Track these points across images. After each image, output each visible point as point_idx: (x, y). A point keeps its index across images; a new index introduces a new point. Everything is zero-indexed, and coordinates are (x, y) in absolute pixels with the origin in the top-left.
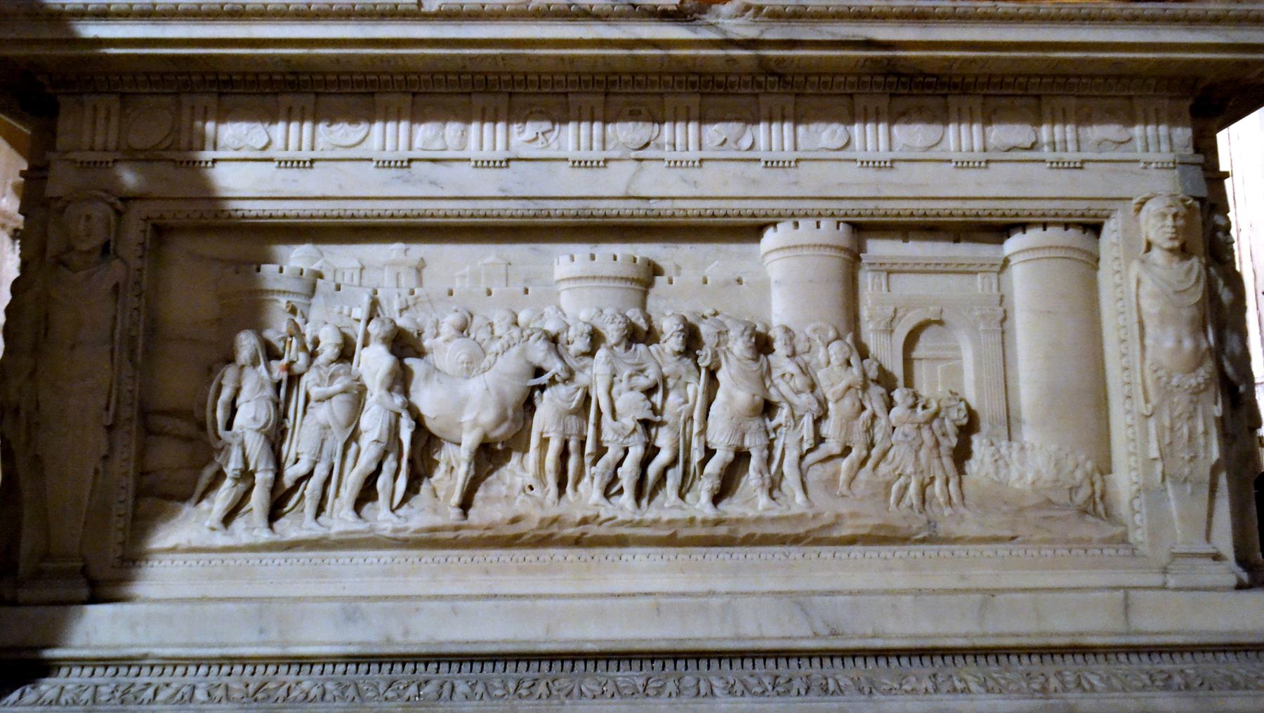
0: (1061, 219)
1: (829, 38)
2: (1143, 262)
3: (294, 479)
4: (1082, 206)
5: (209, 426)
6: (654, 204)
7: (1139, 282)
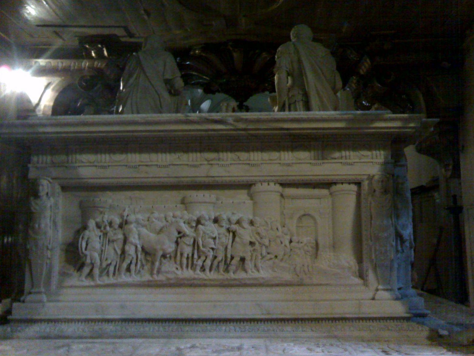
0: (347, 181)
2: (372, 196)
4: (354, 177)
6: (196, 179)
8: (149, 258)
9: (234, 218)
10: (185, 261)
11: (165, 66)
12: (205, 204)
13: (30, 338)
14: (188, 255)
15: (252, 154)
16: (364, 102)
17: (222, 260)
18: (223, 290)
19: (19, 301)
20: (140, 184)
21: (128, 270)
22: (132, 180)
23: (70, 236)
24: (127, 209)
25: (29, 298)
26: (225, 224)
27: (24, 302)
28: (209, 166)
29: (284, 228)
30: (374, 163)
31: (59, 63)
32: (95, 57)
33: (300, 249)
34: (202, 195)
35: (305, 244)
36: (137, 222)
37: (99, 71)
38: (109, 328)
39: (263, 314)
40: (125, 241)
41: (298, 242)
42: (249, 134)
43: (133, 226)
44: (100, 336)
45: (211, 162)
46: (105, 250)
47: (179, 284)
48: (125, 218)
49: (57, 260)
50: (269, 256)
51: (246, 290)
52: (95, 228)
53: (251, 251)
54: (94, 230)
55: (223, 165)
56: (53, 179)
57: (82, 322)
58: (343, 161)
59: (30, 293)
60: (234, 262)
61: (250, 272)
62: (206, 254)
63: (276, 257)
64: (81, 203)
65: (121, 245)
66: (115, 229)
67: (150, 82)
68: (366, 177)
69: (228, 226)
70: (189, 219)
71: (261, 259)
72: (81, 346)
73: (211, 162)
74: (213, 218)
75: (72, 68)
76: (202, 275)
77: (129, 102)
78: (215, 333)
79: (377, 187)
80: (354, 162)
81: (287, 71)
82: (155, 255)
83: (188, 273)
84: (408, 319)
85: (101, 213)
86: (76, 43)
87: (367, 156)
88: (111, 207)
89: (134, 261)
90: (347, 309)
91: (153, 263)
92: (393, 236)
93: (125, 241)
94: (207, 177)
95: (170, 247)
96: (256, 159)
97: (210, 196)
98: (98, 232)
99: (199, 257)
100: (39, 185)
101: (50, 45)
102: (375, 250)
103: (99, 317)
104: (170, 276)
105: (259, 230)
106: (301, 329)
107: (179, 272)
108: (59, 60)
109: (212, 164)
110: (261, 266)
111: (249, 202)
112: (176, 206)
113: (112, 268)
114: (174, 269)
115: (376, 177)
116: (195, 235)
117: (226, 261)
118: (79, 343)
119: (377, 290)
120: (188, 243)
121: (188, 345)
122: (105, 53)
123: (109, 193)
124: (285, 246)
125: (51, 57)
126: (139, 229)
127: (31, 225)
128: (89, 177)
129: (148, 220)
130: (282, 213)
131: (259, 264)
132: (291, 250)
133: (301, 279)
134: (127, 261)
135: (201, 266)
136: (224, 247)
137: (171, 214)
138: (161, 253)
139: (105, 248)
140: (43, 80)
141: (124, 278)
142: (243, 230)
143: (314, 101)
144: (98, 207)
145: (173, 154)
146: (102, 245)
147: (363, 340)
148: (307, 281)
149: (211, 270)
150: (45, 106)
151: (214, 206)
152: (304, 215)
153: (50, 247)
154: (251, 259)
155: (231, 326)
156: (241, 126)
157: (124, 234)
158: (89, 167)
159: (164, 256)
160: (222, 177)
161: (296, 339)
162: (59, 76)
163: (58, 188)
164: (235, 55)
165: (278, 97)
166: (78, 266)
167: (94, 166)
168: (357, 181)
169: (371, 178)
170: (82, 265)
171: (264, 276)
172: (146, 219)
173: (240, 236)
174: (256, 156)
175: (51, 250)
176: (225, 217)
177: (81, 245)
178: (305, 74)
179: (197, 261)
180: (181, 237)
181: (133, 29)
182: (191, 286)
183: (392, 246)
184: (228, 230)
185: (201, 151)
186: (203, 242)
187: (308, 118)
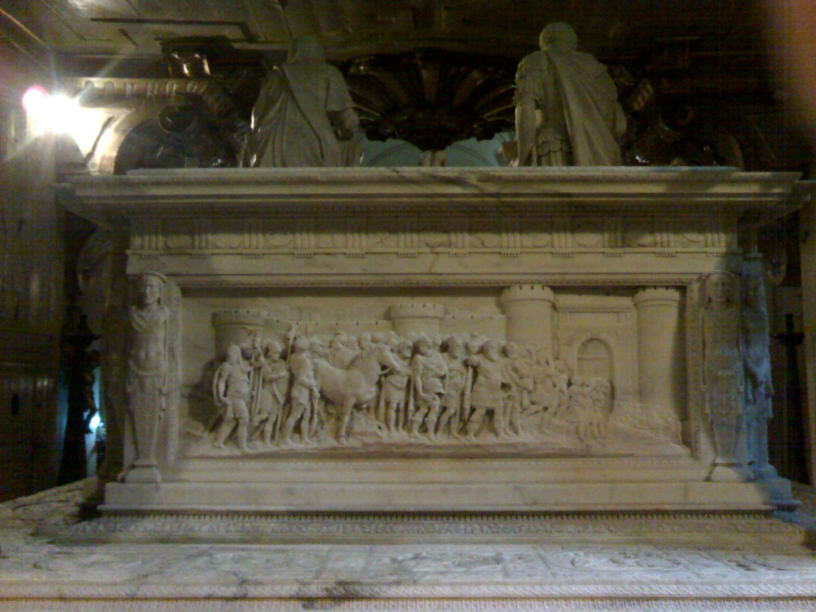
1: (536, 192)
2: (706, 308)
3: (308, 401)
5: (215, 394)
7: (703, 320)
8: (331, 410)
9: (476, 344)
10: (393, 415)
11: (328, 89)
12: (425, 320)
13: (138, 542)
14: (398, 404)
15: (504, 236)
16: (637, 158)
17: (455, 414)
18: (458, 464)
19: (114, 480)
20: (344, 285)
21: (298, 429)
22: (276, 278)
23: (196, 373)
24: (294, 327)
25: (133, 475)
26: (460, 354)
27: (123, 481)
28: (433, 256)
29: (557, 361)
30: (709, 255)
31: (129, 85)
32: (188, 75)
33: (584, 396)
34: (421, 305)
35: (594, 389)
36: (312, 350)
37: (195, 99)
38: (269, 525)
39: (526, 504)
40: (292, 380)
41: (582, 385)
42: (501, 202)
43: (305, 356)
44: (254, 539)
45: (438, 250)
46: (257, 395)
47: (384, 453)
48: (291, 342)
49: (175, 410)
50: (534, 408)
51: (496, 464)
52: (241, 358)
53: (503, 400)
54: (238, 363)
55: (456, 255)
56: (167, 275)
57: (222, 516)
58: (658, 249)
59: (133, 467)
60: (477, 416)
61: (503, 434)
62: (429, 404)
63: (546, 409)
64: (215, 316)
65: (284, 386)
66: (275, 361)
67: (304, 116)
68: (695, 277)
69: (464, 358)
70: (399, 346)
71: (521, 412)
72: (230, 555)
73: (438, 250)
74: (440, 343)
75: (149, 94)
76: (422, 439)
77: (269, 151)
78: (449, 534)
79: (713, 291)
80: (676, 253)
81: (536, 101)
82: (342, 405)
83: (398, 436)
84: (767, 514)
85: (250, 333)
86: (155, 49)
87: (696, 242)
88: (268, 324)
89: (307, 415)
90: (668, 498)
91: (339, 419)
92: (741, 375)
93: (292, 380)
94: (431, 274)
95: (368, 392)
96: (512, 245)
97: (434, 307)
98: (245, 366)
99: (417, 408)
100: (146, 286)
101: (112, 54)
102: (712, 399)
103: (252, 508)
104: (370, 440)
105: (517, 364)
106: (591, 528)
107: (384, 434)
108: (126, 80)
109: (437, 253)
110: (521, 425)
111: (499, 317)
112: (377, 323)
113: (269, 427)
114: (375, 429)
115: (714, 278)
116: (409, 372)
117: (462, 414)
118: (224, 550)
119: (715, 465)
120: (399, 385)
121: (410, 555)
122: (207, 68)
123: (263, 300)
124: (561, 391)
125: (108, 76)
126: (316, 360)
127: (133, 352)
128: (229, 273)
129: (330, 347)
130: (555, 337)
131: (519, 422)
132: (570, 397)
133: (587, 446)
134: (296, 415)
135: (420, 423)
136: (460, 392)
137: (369, 337)
138: (352, 401)
139: (257, 393)
140: (101, 114)
141: (291, 443)
142: (491, 364)
143: (582, 150)
144: (244, 323)
145: (372, 236)
146: (253, 389)
147: (695, 547)
148: (596, 449)
149: (436, 430)
150: (103, 158)
151: (440, 324)
152: (591, 340)
153: (165, 390)
154: (504, 414)
155: (475, 524)
156: (491, 188)
157: (290, 370)
158: (230, 256)
159: (358, 407)
160: (454, 274)
161: (585, 545)
162: (128, 107)
163: (176, 292)
164: (426, 74)
165: (519, 146)
166: (211, 423)
167: (238, 254)
168: (679, 284)
169: (703, 279)
170: (219, 421)
171: (527, 441)
172: (327, 344)
173: (485, 373)
174: (513, 241)
175: (167, 395)
176: (460, 341)
177: (217, 386)
178: (567, 104)
179: (413, 415)
180: (386, 376)
181: (257, 28)
182: (406, 456)
183: (740, 393)
184: (466, 364)
185: (419, 231)
186: (423, 382)
187: (604, 176)
